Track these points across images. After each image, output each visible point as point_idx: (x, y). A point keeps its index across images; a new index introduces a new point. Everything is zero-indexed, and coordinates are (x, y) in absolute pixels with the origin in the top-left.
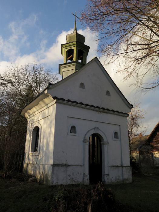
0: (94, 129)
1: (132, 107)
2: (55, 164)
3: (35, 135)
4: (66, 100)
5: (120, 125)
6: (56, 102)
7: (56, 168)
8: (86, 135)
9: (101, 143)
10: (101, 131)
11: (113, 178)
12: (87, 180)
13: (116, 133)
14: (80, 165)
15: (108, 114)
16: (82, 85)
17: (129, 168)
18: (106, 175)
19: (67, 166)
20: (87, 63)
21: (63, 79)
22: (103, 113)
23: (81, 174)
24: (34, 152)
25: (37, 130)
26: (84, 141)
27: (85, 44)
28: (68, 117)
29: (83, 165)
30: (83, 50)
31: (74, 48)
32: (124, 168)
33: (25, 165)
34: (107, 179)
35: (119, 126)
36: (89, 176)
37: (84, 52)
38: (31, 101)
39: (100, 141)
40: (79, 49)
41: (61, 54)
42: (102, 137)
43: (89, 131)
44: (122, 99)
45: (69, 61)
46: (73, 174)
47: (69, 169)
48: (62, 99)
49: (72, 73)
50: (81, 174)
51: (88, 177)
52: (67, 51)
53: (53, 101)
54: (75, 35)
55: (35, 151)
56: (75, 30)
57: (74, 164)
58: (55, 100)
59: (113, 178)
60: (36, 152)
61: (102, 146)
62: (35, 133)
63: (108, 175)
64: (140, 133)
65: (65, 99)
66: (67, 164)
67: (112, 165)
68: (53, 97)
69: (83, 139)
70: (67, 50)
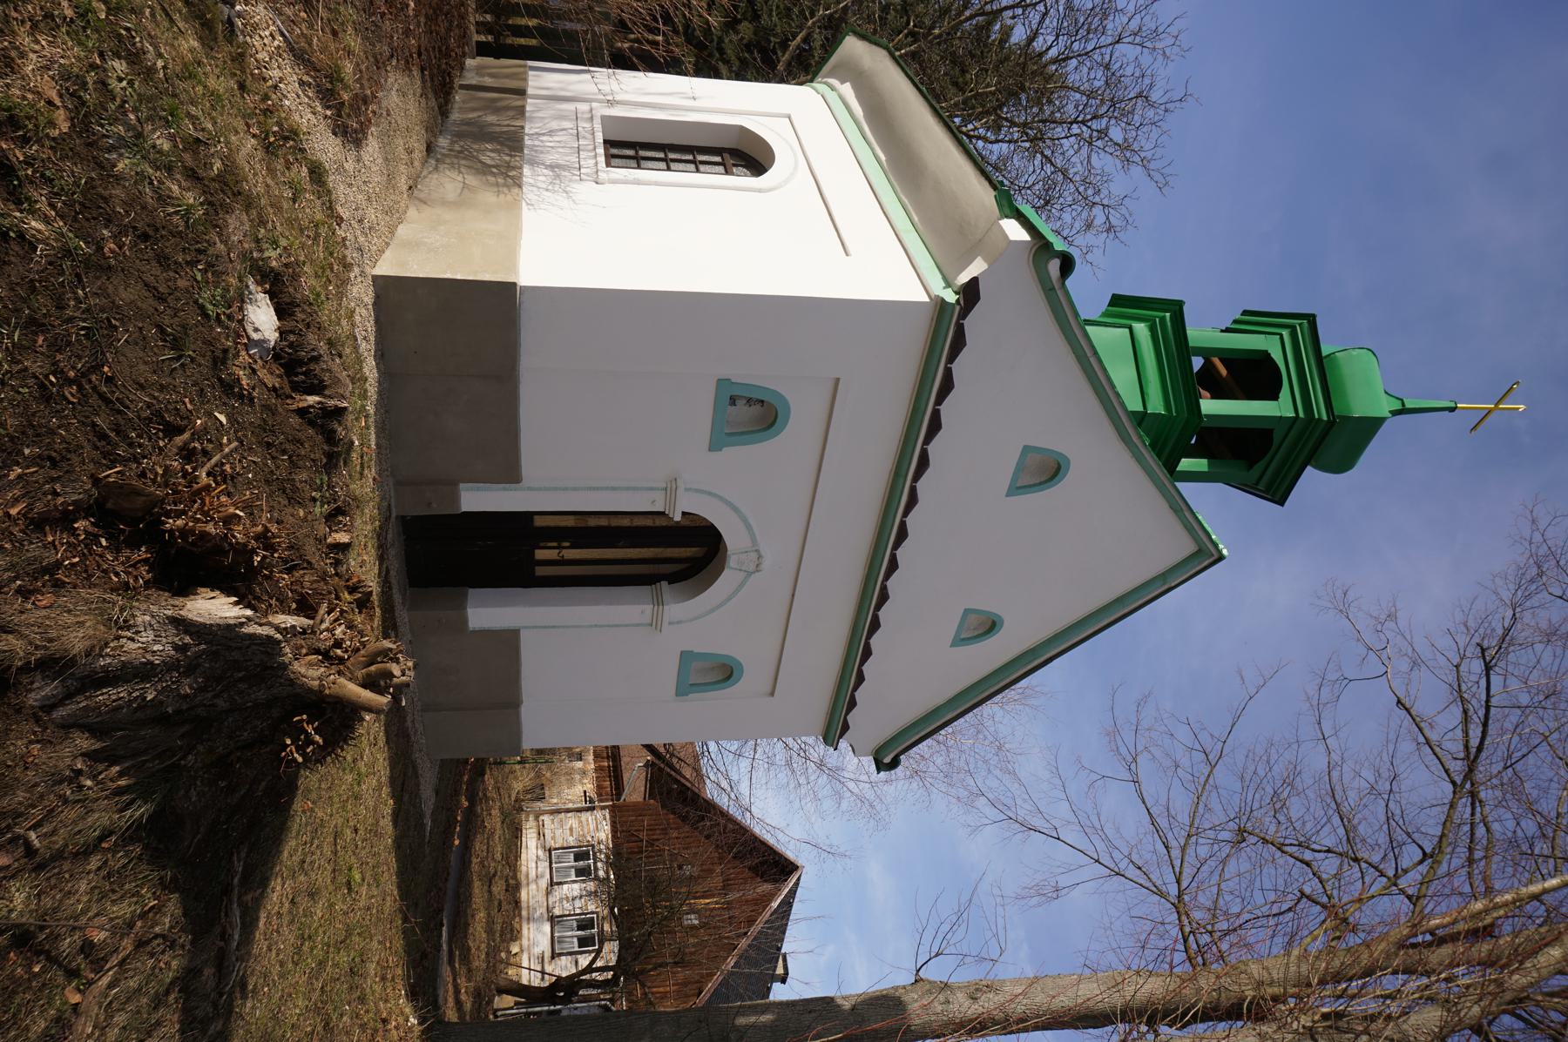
1: (880, 766)
4: (939, 410)
5: (772, 694)
6: (942, 303)
13: (726, 673)
20: (1177, 484)
21: (1089, 329)
24: (600, 139)
27: (1309, 469)
28: (838, 380)
30: (1262, 463)
31: (1280, 408)
37: (1251, 465)
38: (917, 80)
39: (673, 579)
40: (1277, 437)
41: (1245, 313)
42: (694, 597)
45: (1197, 363)
48: (959, 343)
49: (1119, 389)
53: (948, 285)
55: (605, 142)
58: (951, 297)
60: (601, 151)
61: (644, 591)
65: (931, 444)
68: (974, 281)
70: (1277, 356)
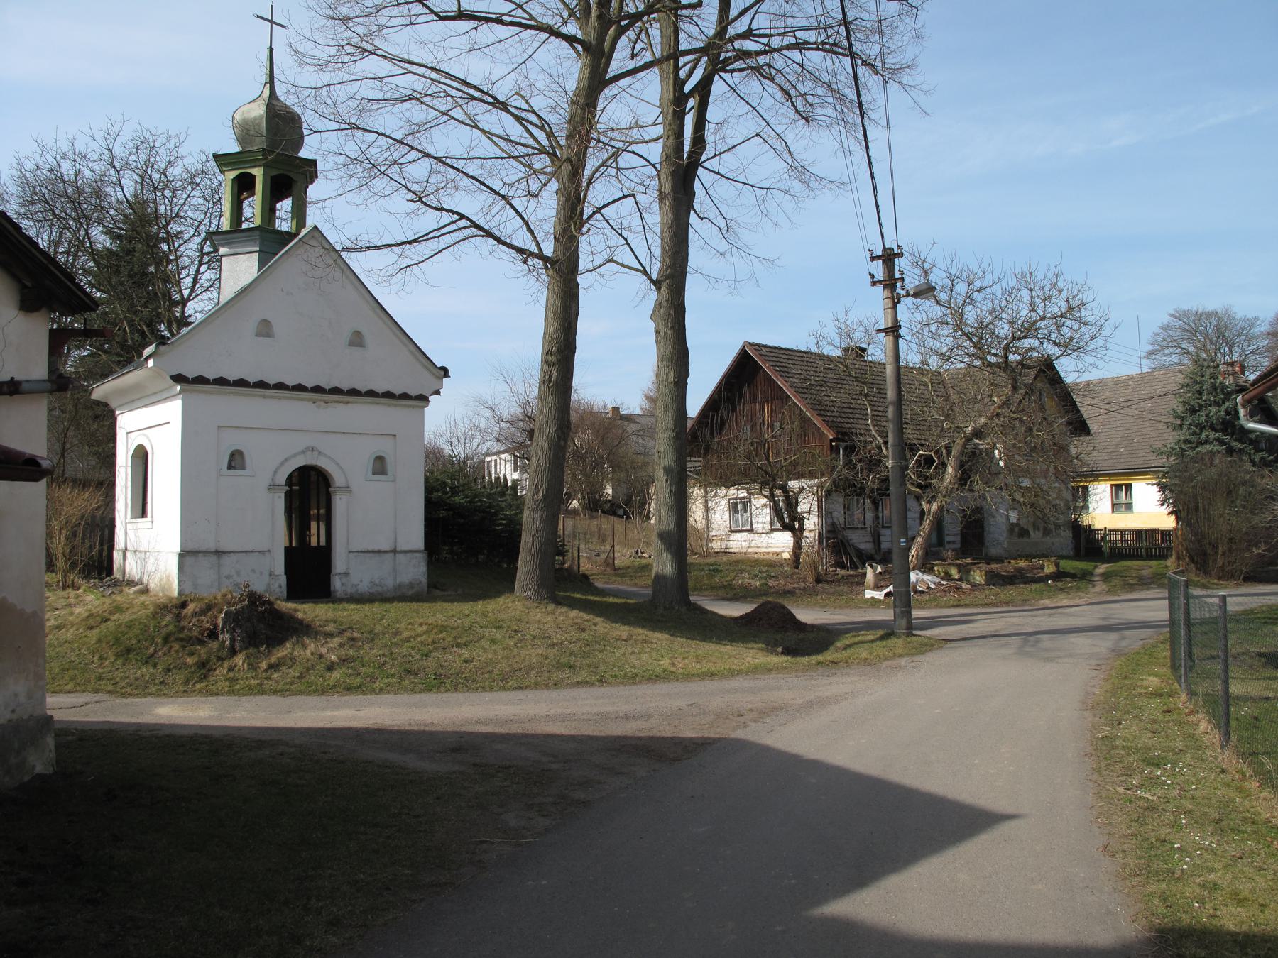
0: (303, 452)
2: (188, 549)
3: (140, 470)
7: (189, 560)
8: (275, 472)
9: (331, 489)
10: (325, 455)
11: (361, 581)
12: (280, 587)
14: (259, 552)
15: (350, 405)
16: (265, 329)
17: (417, 555)
18: (340, 574)
19: (219, 553)
22: (336, 405)
23: (261, 573)
25: (141, 457)
26: (273, 486)
29: (269, 551)
32: (400, 557)
33: (117, 556)
34: (343, 585)
35: (392, 437)
36: (284, 578)
40: (274, 173)
43: (286, 460)
44: (412, 353)
46: (238, 573)
47: (226, 560)
48: (201, 380)
50: (261, 573)
51: (283, 580)
52: (234, 180)
54: (261, 117)
55: (143, 517)
56: (268, 85)
57: (240, 550)
59: (361, 581)
62: (140, 462)
63: (346, 574)
64: (49, 574)
66: (219, 549)
67: (360, 550)
69: (268, 482)
